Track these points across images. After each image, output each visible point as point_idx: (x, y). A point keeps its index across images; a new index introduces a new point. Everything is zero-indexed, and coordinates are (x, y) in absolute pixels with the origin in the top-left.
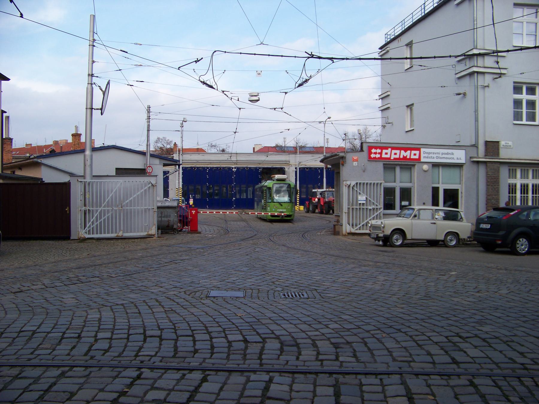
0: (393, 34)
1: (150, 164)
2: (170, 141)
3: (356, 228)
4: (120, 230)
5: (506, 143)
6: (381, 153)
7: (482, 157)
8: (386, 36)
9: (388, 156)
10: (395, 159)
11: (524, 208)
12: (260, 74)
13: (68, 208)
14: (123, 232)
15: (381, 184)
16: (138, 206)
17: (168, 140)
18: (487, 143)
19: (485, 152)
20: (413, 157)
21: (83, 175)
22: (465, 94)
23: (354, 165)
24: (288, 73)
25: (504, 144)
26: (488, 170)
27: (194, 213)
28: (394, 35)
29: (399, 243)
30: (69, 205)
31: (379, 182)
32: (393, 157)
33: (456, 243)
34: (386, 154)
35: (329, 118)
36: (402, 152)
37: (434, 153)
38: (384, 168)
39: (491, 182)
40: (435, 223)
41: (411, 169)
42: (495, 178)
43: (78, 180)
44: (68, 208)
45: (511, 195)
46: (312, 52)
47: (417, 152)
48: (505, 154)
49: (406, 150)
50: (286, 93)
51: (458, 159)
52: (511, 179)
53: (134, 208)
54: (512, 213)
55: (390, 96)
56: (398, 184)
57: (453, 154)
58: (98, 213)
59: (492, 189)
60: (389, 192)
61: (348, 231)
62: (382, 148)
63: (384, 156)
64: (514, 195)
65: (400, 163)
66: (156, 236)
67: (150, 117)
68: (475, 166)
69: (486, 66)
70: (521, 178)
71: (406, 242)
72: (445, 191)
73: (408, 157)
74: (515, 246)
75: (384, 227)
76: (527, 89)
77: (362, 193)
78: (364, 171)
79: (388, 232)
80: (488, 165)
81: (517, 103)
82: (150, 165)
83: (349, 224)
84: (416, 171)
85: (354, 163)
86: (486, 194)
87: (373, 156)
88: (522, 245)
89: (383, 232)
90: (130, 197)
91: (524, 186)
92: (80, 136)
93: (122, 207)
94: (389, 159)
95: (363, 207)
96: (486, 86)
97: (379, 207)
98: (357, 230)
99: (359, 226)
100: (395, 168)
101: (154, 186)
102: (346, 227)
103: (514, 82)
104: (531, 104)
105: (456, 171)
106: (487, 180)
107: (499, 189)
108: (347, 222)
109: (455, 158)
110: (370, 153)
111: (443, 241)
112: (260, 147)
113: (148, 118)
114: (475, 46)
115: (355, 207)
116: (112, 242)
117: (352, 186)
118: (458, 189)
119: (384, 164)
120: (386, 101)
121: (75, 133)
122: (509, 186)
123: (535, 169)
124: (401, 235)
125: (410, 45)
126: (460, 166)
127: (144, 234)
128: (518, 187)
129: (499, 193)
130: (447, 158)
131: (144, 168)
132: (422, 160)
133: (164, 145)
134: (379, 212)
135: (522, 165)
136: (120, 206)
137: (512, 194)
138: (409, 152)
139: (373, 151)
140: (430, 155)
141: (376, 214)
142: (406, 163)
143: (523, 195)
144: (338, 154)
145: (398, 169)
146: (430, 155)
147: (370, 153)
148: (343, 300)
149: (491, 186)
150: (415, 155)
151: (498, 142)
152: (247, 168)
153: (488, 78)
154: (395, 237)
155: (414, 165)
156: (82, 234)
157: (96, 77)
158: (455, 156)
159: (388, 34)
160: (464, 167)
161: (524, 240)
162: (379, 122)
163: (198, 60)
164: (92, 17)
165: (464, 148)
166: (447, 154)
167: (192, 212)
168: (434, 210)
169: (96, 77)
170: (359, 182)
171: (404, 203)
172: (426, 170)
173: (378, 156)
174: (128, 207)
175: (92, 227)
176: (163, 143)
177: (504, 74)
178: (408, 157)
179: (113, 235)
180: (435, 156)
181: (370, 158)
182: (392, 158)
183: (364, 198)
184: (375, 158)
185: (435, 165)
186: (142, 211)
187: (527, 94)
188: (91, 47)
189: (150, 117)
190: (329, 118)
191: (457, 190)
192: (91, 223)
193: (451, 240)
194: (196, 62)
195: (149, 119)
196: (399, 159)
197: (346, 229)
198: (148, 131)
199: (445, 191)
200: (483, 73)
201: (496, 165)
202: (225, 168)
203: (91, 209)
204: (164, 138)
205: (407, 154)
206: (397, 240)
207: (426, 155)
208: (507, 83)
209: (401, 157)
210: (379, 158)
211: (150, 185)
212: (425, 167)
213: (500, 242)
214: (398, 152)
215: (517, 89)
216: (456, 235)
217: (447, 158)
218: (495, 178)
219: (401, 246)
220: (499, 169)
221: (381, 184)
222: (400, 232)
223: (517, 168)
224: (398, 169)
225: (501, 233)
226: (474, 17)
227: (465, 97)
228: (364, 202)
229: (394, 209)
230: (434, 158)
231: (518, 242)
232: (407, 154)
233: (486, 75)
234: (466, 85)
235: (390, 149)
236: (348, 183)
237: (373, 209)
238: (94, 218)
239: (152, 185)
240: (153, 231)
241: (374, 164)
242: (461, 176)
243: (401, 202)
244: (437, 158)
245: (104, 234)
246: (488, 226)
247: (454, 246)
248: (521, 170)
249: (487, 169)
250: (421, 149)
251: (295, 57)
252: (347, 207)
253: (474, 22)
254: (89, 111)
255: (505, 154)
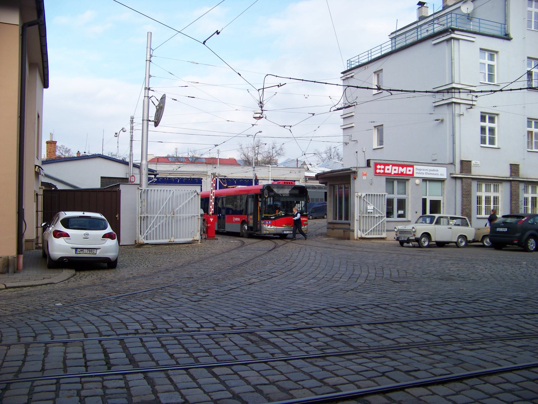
0: (357, 61)
1: (132, 174)
2: (68, 149)
3: (366, 234)
4: (171, 236)
5: (476, 162)
6: (384, 169)
7: (458, 173)
8: (349, 62)
9: (389, 172)
10: (395, 174)
11: (533, 216)
12: (307, 98)
13: (118, 214)
14: (174, 238)
15: (385, 195)
16: (186, 214)
17: (66, 148)
18: (462, 162)
19: (461, 170)
20: (408, 173)
21: (139, 183)
22: (442, 121)
23: (364, 179)
24: (331, 98)
25: (475, 163)
26: (464, 184)
27: (211, 221)
28: (358, 62)
29: (426, 244)
30: (119, 212)
31: (384, 194)
32: (393, 172)
33: (465, 245)
34: (388, 169)
35: (260, 132)
36: (400, 168)
37: (423, 170)
38: (386, 181)
39: (466, 194)
40: (451, 228)
41: (405, 183)
42: (468, 191)
43: (138, 188)
44: (118, 214)
45: (479, 205)
46: (380, 86)
47: (411, 169)
48: (476, 171)
49: (403, 166)
50: (313, 114)
51: (441, 175)
52: (479, 192)
53: (180, 215)
54: (523, 220)
55: (354, 116)
56: (396, 197)
57: (438, 171)
58: (155, 219)
59: (466, 200)
60: (390, 202)
61: (359, 236)
62: (385, 165)
63: (386, 171)
64: (489, 206)
65: (398, 178)
66: (199, 241)
67: (133, 128)
68: (453, 181)
69: (462, 98)
70: (486, 191)
71: (431, 243)
72: (431, 201)
73: (405, 173)
74: (527, 244)
75: (415, 232)
76: (490, 118)
77: (370, 204)
78: (371, 184)
79: (418, 235)
80: (464, 180)
81: (483, 129)
82: (133, 175)
83: (360, 230)
84: (410, 186)
85: (364, 177)
86: (462, 205)
87: (378, 171)
88: (532, 243)
89: (414, 235)
90: (180, 205)
91: (488, 198)
92: (55, 144)
93: (174, 215)
94: (390, 174)
95: (371, 215)
96: (461, 115)
97: (383, 215)
98: (366, 235)
99: (368, 232)
100: (393, 182)
101: (198, 195)
102: (357, 232)
103: (481, 112)
104: (492, 130)
105: (439, 185)
106: (462, 193)
107: (471, 200)
108: (358, 228)
109: (439, 174)
110: (376, 169)
111: (456, 243)
112: (152, 157)
113: (132, 128)
114: (453, 81)
115: (365, 215)
116: (160, 247)
117: (363, 196)
118: (426, 198)
119: (386, 179)
120: (349, 121)
121: (49, 140)
122: (478, 198)
123: (495, 184)
124: (427, 237)
125: (378, 73)
126: (442, 181)
127: (190, 239)
128: (483, 199)
129: (471, 203)
130: (433, 174)
131: (125, 177)
132: (415, 175)
133: (62, 154)
134: (384, 219)
135: (497, 182)
136: (172, 213)
137: (496, 205)
138: (405, 168)
139: (378, 167)
140: (421, 172)
141: (381, 221)
142: (403, 178)
143: (487, 206)
144: (351, 169)
145: (396, 183)
146: (421, 172)
147: (376, 169)
148: (395, 293)
149: (466, 197)
150: (410, 171)
151: (471, 161)
152: (190, 179)
153: (463, 107)
154: (423, 240)
155: (408, 180)
156: (141, 240)
157: (152, 90)
158: (439, 173)
159: (351, 60)
160: (446, 182)
161: (533, 240)
162: (341, 139)
163: (281, 85)
164: (149, 34)
165: (446, 166)
166: (434, 170)
167: (210, 219)
168: (449, 218)
169: (152, 90)
170: (368, 193)
171: (401, 212)
172: (418, 184)
173: (382, 171)
174: (178, 214)
175: (149, 232)
176: (61, 151)
177: (474, 105)
178: (405, 173)
179: (166, 241)
180: (424, 172)
181: (376, 173)
182: (393, 173)
183: (372, 207)
184: (379, 173)
185: (425, 180)
186: (186, 219)
187: (489, 122)
188: (148, 62)
189: (133, 128)
190: (260, 132)
191: (440, 201)
192: (148, 229)
193: (461, 242)
194: (278, 86)
195: (133, 129)
196: (398, 174)
197: (357, 234)
198: (132, 141)
199: (431, 201)
200: (459, 104)
201: (469, 180)
202: (171, 178)
203: (149, 215)
204: (62, 146)
205: (404, 170)
206: (424, 242)
207: (418, 171)
208: (476, 113)
209: (400, 172)
210: (383, 173)
211: (196, 193)
212: (418, 181)
213: (516, 242)
214: (397, 168)
215: (483, 119)
216: (464, 237)
217: (433, 174)
218: (468, 191)
219: (429, 246)
220: (471, 184)
221: (385, 195)
222: (427, 235)
223: (483, 183)
224: (396, 183)
225: (518, 235)
226: (452, 57)
227: (443, 123)
228: (372, 211)
229: (348, 220)
230: (424, 174)
231: (529, 242)
232: (404, 170)
233: (461, 105)
234: (445, 113)
235: (391, 166)
236: (360, 194)
237: (379, 217)
238: (152, 224)
239: (197, 194)
240: (198, 237)
241: (379, 178)
242: (443, 189)
243: (398, 212)
244: (426, 174)
245: (165, 239)
246: (506, 230)
247: (464, 247)
248: (532, 187)
249: (462, 183)
250: (414, 166)
251: (337, 85)
252: (358, 215)
253: (452, 61)
254: (145, 122)
255: (476, 171)
